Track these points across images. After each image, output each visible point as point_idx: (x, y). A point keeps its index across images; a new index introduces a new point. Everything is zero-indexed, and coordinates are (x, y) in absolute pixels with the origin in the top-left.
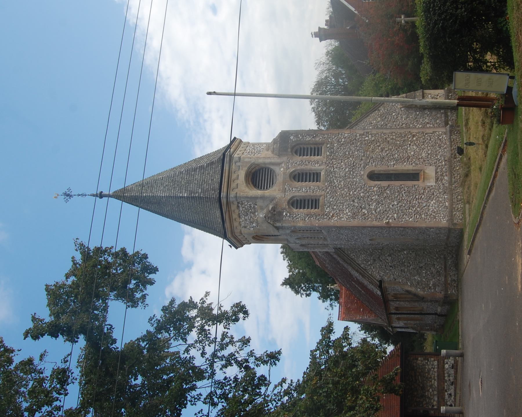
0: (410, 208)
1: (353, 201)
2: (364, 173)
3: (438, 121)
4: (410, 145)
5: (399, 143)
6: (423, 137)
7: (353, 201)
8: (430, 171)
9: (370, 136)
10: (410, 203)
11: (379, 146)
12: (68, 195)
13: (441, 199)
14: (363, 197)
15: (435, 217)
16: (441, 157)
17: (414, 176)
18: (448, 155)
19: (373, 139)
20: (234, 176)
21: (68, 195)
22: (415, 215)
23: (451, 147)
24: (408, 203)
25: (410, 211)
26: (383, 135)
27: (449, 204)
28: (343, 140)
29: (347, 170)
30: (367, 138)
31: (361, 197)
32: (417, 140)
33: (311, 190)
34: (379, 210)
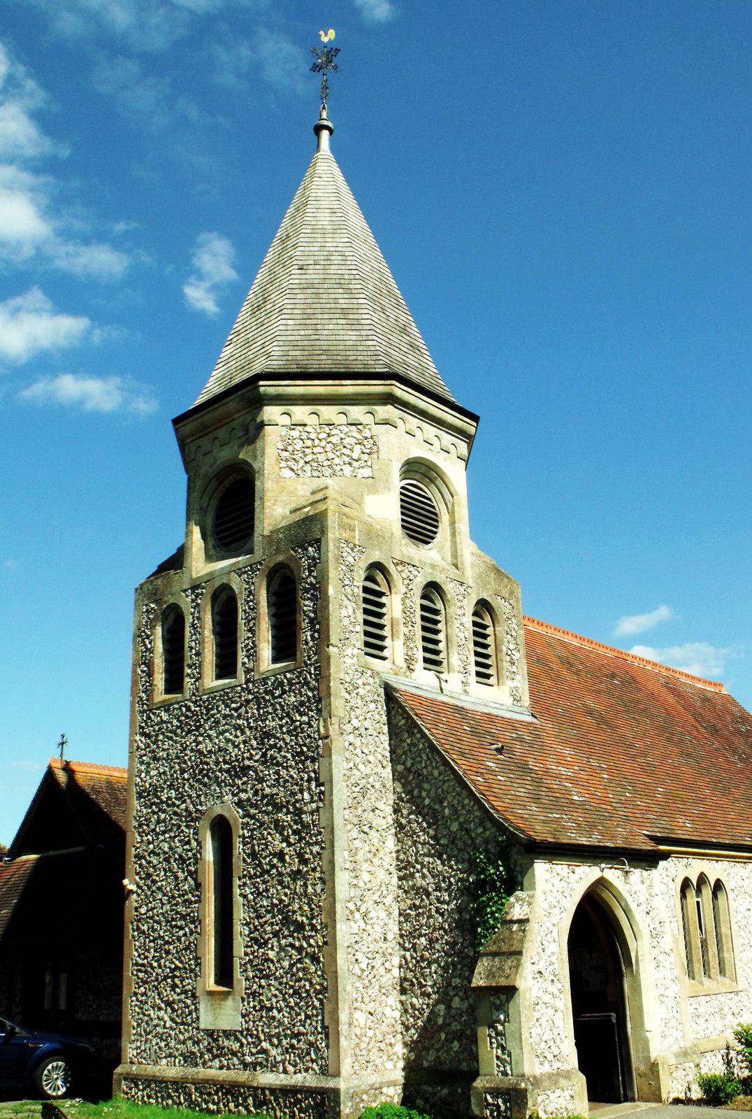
3: (456, 1044)
28: (305, 719)
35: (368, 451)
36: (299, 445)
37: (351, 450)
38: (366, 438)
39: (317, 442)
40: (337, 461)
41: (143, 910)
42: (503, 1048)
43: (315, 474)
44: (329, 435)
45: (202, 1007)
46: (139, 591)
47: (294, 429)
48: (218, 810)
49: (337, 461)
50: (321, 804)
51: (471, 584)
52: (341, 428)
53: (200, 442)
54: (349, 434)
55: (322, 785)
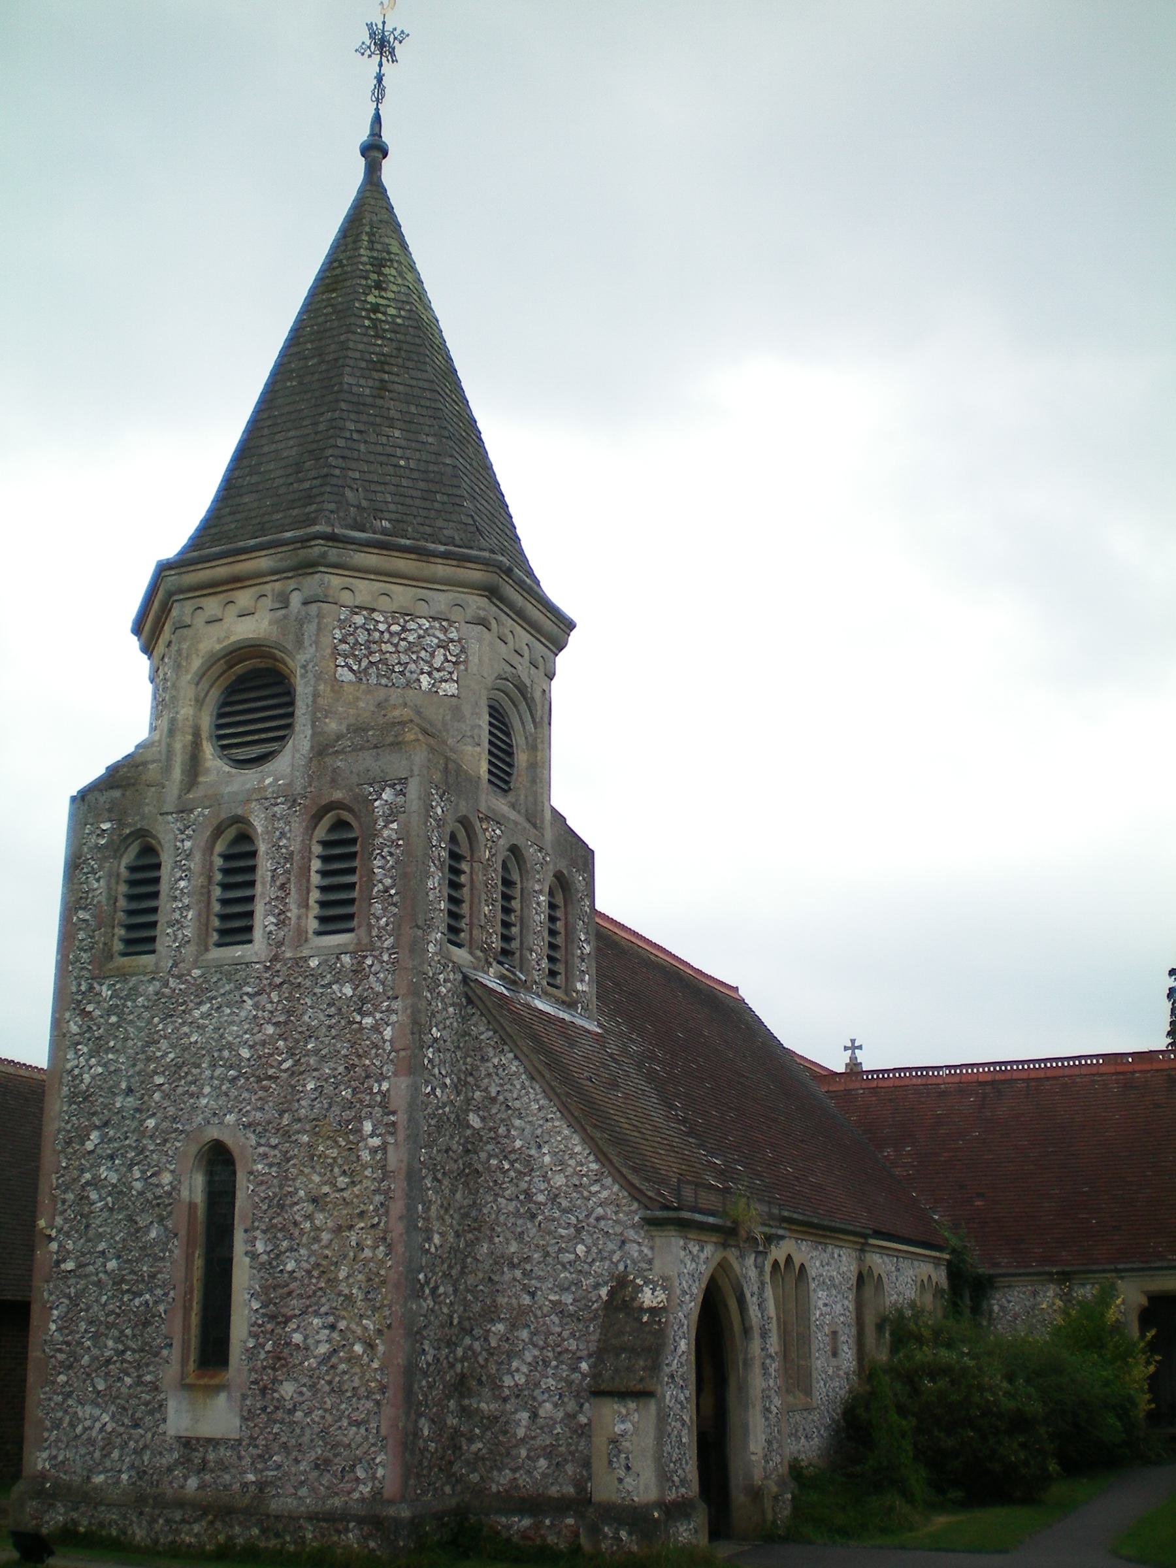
0: (91, 1323)
1: (130, 1091)
2: (227, 1128)
4: (333, 1327)
5: (342, 1275)
6: (362, 1391)
7: (130, 1091)
8: (220, 1417)
9: (375, 1142)
10: (109, 1326)
11: (333, 1185)
12: (382, 44)
13: (116, 1454)
14: (141, 1132)
15: (57, 1425)
16: (279, 1467)
17: (213, 1350)
18: (282, 1503)
19: (365, 1156)
20: (244, 598)
21: (382, 44)
22: (68, 1344)
23: (312, 1517)
24: (111, 1318)
25: (83, 1326)
26: (378, 1198)
27: (96, 1488)
28: (368, 1021)
29: (245, 1053)
30: (368, 1127)
31: (142, 1122)
32: (352, 1359)
33: (177, 916)
34: (94, 1196)
35: (454, 659)
36: (362, 637)
37: (432, 655)
38: (452, 641)
39: (386, 636)
40: (412, 666)
41: (70, 1265)
42: (628, 1468)
43: (384, 681)
44: (404, 629)
45: (172, 1406)
46: (79, 801)
47: (356, 614)
48: (214, 1133)
49: (412, 666)
50: (391, 1140)
51: (550, 851)
52: (419, 620)
53: (203, 602)
54: (431, 631)
55: (394, 1113)
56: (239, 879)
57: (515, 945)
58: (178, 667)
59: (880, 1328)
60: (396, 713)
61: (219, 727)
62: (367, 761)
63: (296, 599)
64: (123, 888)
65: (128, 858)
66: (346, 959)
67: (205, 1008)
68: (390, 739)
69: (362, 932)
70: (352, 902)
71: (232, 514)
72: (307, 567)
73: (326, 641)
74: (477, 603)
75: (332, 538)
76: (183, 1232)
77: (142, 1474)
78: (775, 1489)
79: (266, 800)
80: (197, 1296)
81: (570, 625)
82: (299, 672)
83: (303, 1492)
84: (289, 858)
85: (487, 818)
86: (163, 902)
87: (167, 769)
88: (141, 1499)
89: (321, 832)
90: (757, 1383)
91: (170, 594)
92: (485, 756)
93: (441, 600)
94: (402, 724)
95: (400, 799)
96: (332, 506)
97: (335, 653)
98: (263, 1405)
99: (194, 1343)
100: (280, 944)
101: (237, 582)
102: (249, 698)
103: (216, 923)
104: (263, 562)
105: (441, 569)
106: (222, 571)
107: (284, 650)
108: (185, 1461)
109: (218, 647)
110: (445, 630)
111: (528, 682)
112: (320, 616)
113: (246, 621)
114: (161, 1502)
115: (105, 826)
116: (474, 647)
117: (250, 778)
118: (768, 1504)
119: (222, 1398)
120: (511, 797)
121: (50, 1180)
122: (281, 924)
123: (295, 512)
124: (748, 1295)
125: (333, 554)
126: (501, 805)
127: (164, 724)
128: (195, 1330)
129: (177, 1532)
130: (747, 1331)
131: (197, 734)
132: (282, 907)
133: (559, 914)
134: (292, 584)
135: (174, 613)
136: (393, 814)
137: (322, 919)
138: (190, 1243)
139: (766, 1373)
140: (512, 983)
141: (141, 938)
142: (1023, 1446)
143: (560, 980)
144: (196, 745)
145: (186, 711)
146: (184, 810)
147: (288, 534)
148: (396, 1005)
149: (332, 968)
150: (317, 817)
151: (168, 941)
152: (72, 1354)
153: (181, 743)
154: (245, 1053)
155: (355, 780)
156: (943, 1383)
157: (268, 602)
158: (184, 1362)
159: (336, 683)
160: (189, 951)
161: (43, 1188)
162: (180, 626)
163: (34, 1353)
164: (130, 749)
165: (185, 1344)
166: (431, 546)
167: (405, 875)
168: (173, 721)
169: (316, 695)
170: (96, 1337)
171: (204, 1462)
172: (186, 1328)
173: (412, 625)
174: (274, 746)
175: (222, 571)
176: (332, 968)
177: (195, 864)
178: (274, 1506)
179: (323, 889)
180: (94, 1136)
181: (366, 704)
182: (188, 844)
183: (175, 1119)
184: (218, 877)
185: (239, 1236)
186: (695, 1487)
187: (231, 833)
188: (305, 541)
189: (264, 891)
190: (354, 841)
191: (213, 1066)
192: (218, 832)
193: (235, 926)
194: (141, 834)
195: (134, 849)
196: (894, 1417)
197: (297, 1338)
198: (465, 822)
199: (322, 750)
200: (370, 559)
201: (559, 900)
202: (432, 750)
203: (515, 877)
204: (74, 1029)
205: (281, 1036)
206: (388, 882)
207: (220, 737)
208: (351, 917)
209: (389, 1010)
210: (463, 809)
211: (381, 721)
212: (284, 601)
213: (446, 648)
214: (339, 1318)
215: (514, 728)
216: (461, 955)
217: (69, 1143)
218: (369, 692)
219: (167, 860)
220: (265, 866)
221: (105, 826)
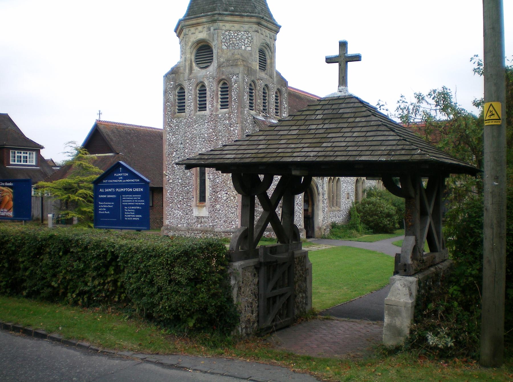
1: (182, 143)
6: (233, 207)
7: (182, 143)
13: (183, 220)
17: (202, 198)
20: (200, 28)
28: (232, 129)
29: (206, 135)
40: (240, 44)
41: (171, 181)
44: (238, 35)
45: (194, 210)
49: (240, 44)
56: (203, 96)
57: (267, 107)
58: (186, 44)
59: (364, 192)
60: (236, 56)
61: (196, 59)
62: (230, 69)
63: (212, 29)
64: (177, 97)
65: (178, 90)
66: (227, 115)
67: (197, 125)
68: (235, 64)
69: (230, 108)
70: (228, 101)
71: (196, 5)
72: (214, 21)
73: (219, 39)
74: (255, 27)
75: (220, 14)
76: (195, 174)
77: (188, 224)
78: (325, 228)
79: (208, 78)
80: (198, 187)
81: (280, 27)
82: (214, 47)
83: (222, 227)
84: (213, 91)
85: (259, 79)
86: (186, 101)
87: (185, 70)
88: (189, 229)
89: (220, 85)
90: (321, 205)
91: (183, 27)
92: (258, 65)
93: (246, 27)
94: (238, 59)
95: (237, 78)
96: (219, 5)
97: (222, 42)
98: (213, 209)
99: (198, 197)
100: (212, 111)
101: (198, 24)
102: (203, 52)
103: (198, 106)
104: (204, 20)
105: (246, 19)
106: (194, 21)
107: (210, 41)
108: (197, 221)
109: (195, 40)
110: (248, 34)
111: (269, 43)
112: (218, 33)
113: (200, 34)
114: (193, 230)
115: (172, 83)
116: (255, 38)
117: (204, 72)
118: (322, 231)
119: (205, 208)
120: (266, 72)
121: (165, 163)
122: (212, 106)
123: (211, 6)
124: (319, 186)
125: (220, 18)
126: (263, 75)
127: (183, 57)
128: (198, 194)
129: (196, 236)
130: (319, 194)
131: (191, 61)
132: (213, 102)
133: (279, 98)
134: (211, 25)
135: (184, 31)
136: (236, 82)
137: (221, 105)
138: (196, 176)
139: (323, 203)
140: (266, 117)
141: (182, 109)
142: (389, 220)
143: (279, 114)
144: (191, 63)
145: (188, 56)
146: (189, 79)
147: (209, 13)
148: (238, 125)
149: (224, 117)
150: (219, 82)
151: (188, 110)
152: (173, 200)
153: (188, 64)
154: (206, 135)
155: (227, 73)
156: (371, 206)
157: (205, 29)
158: (196, 201)
159: (222, 50)
160: (193, 112)
161: (164, 164)
162: (185, 35)
163: (164, 200)
164: (176, 63)
165: (196, 197)
166: (243, 14)
167: (239, 96)
168: (185, 58)
169: (218, 53)
170: (177, 196)
171: (201, 221)
172: (196, 194)
173: (240, 33)
174: (209, 64)
175: (194, 21)
176: (224, 117)
177: (193, 92)
178: (216, 230)
179: (221, 98)
180: (174, 153)
181: (230, 54)
182: (191, 88)
183: (192, 150)
184: (198, 95)
185: (207, 177)
186: (303, 226)
187: (200, 85)
188: (213, 15)
189: (208, 99)
190: (228, 88)
191: (199, 138)
192: (197, 85)
193: (202, 107)
194: (180, 85)
195: (179, 88)
196: (356, 213)
197: (219, 196)
198: (253, 81)
199: (219, 66)
200: (229, 18)
201: (279, 95)
202: (244, 66)
203: (267, 91)
204: (168, 130)
205: (214, 132)
206: (235, 97)
207: (197, 61)
208: (228, 105)
209: (236, 126)
210: (253, 78)
211: (233, 58)
212: (209, 29)
213: (248, 38)
214: (228, 192)
215: (265, 55)
216: (253, 112)
217: (169, 155)
218: (230, 51)
219: (186, 91)
220: (208, 93)
221: (172, 83)
